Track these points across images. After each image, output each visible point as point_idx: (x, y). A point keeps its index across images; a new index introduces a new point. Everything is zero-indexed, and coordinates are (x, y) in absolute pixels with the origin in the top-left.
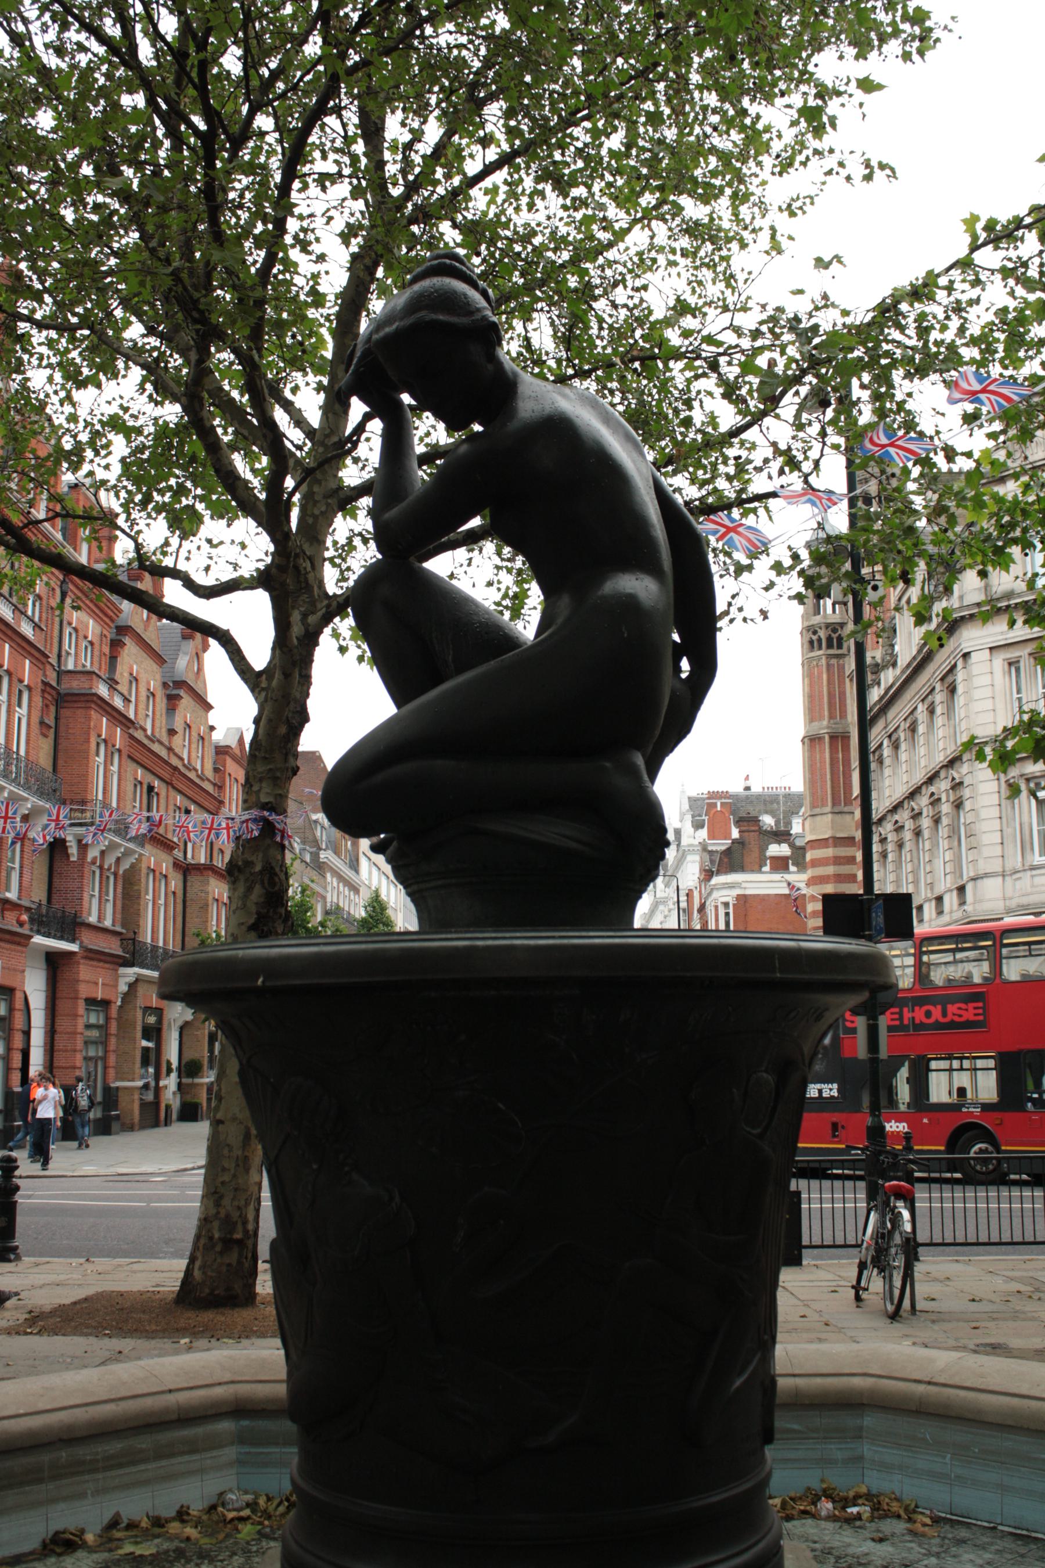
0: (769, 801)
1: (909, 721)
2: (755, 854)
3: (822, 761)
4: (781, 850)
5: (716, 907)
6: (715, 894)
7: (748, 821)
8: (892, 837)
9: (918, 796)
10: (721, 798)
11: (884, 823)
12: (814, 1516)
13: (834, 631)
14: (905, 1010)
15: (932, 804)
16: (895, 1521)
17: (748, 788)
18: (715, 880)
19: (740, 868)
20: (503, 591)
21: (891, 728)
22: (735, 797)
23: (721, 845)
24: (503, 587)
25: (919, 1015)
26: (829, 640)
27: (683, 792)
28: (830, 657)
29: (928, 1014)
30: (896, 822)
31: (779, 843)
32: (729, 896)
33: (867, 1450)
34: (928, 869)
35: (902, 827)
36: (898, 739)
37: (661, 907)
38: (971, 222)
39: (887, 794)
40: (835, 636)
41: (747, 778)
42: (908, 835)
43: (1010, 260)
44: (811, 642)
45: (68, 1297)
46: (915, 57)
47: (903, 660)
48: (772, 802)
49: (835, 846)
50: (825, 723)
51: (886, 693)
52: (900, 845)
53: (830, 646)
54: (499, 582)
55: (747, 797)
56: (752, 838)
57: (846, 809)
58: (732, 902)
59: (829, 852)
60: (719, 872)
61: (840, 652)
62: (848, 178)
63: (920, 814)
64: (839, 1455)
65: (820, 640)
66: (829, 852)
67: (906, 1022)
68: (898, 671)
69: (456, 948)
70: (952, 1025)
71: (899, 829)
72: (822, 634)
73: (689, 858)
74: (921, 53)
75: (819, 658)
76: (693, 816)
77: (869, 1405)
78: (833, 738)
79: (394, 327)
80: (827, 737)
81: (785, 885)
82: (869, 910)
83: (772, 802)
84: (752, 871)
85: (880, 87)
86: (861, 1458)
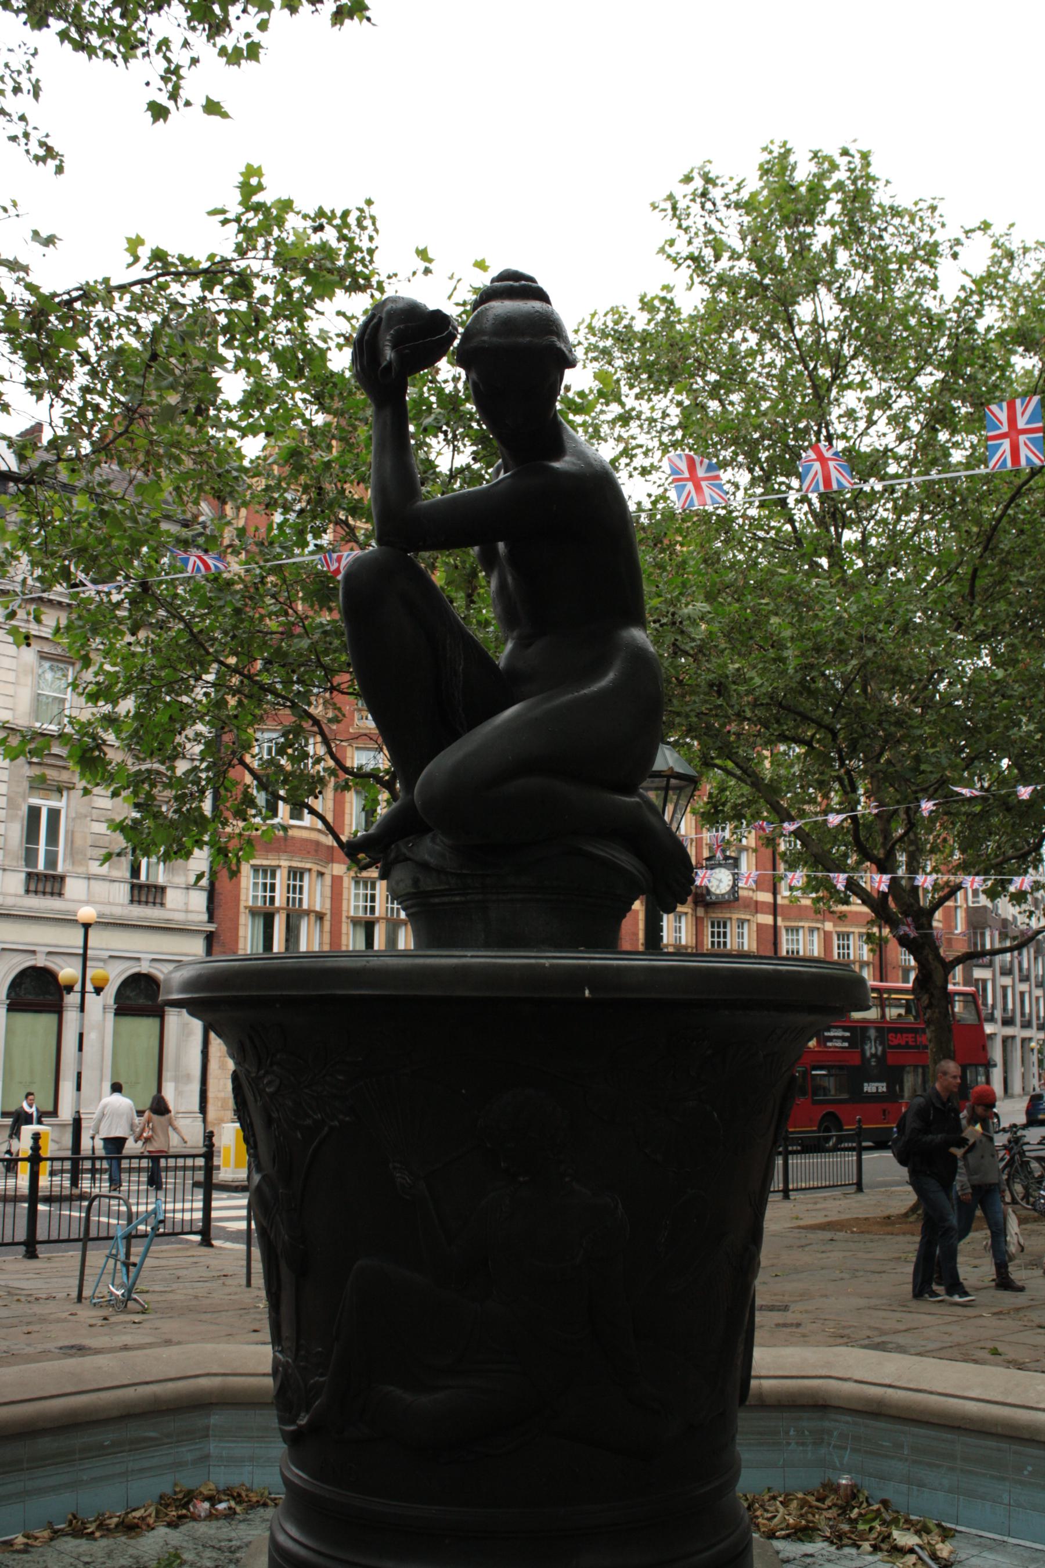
12: (195, 1518)
16: (261, 1510)
33: (213, 1447)
38: (134, 244)
43: (183, 296)
45: (100, 1356)
46: (120, 60)
64: (189, 1457)
69: (514, 965)
77: (217, 1404)
85: (225, 115)
86: (207, 1457)
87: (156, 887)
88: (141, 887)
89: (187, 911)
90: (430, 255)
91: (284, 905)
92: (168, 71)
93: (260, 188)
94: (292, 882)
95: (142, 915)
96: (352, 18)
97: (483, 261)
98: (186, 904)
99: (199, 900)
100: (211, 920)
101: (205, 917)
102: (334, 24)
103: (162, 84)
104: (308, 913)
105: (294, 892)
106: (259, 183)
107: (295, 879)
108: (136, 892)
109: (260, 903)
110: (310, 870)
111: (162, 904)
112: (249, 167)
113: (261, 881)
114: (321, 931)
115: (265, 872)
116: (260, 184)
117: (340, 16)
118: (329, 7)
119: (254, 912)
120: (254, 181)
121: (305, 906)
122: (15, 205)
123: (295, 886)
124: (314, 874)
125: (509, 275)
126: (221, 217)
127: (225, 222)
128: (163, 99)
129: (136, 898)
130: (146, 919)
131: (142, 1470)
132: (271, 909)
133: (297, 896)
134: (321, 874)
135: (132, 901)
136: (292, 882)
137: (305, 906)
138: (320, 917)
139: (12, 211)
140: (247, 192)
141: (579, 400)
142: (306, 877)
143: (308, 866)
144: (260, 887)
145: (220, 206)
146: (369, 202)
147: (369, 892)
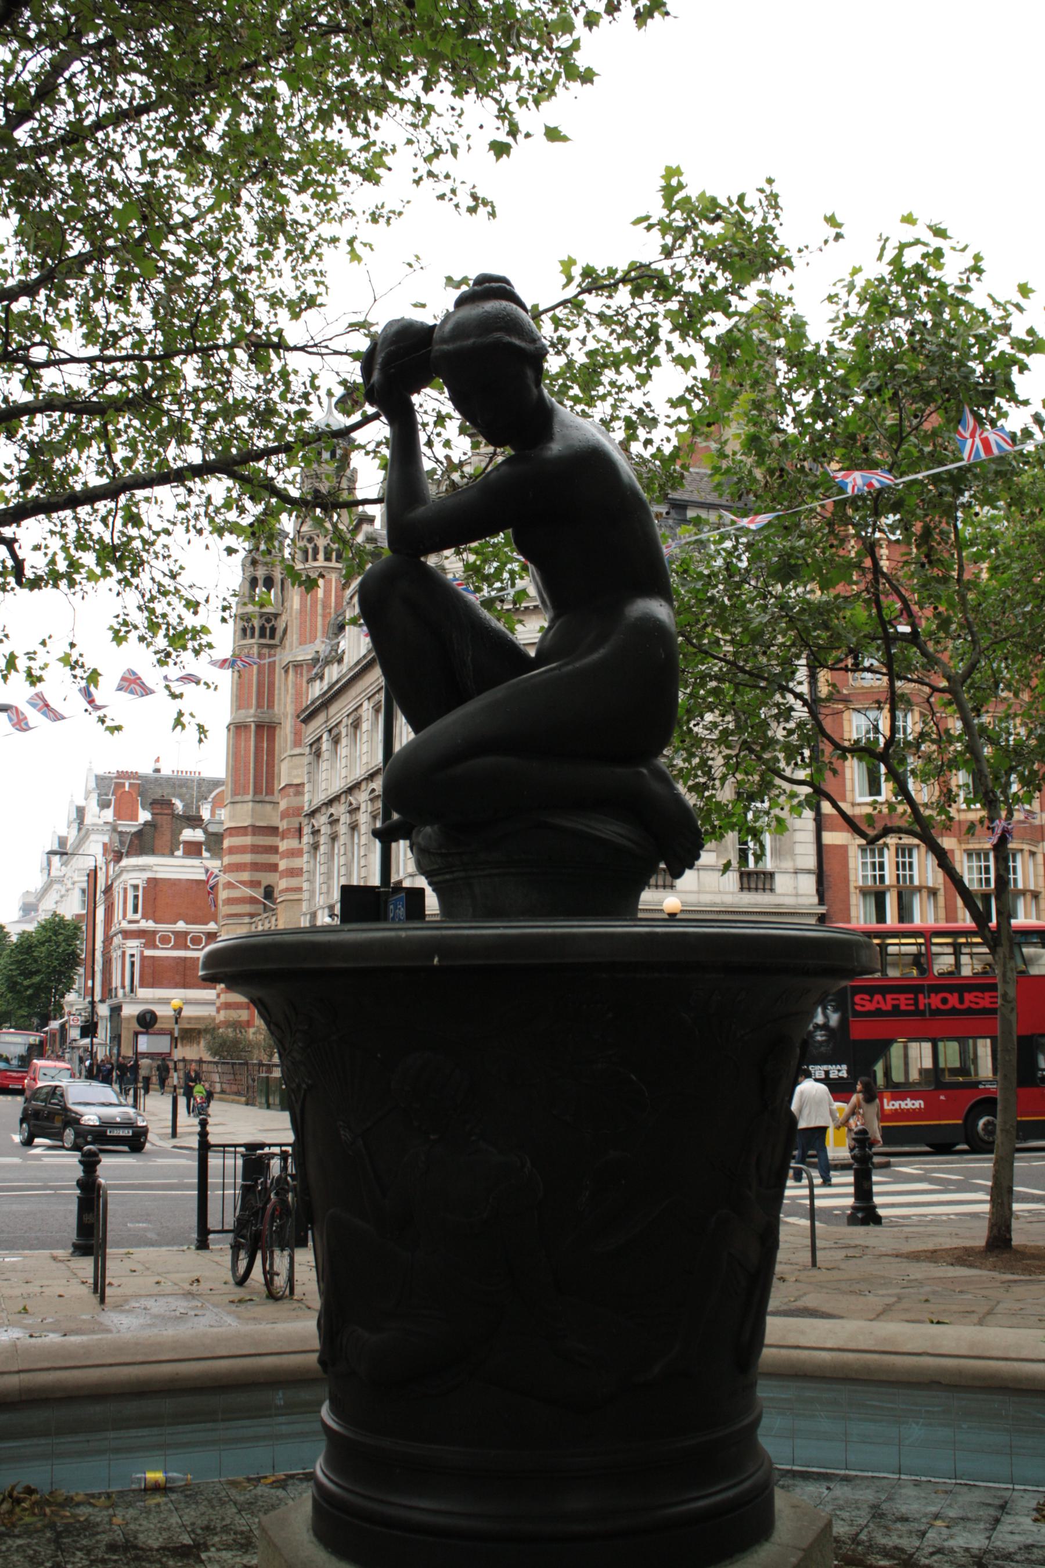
0: (180, 784)
1: (352, 717)
2: (167, 836)
3: (247, 749)
4: (196, 835)
5: (125, 890)
6: (125, 876)
7: (160, 805)
8: (325, 830)
9: (356, 792)
10: (129, 778)
11: (317, 816)
13: (268, 620)
14: (921, 996)
15: (371, 800)
17: (157, 771)
18: (125, 862)
19: (152, 851)
20: (49, 556)
21: (332, 723)
22: (144, 778)
23: (130, 827)
24: (50, 552)
25: (935, 1001)
26: (263, 629)
27: (90, 769)
28: (262, 646)
29: (944, 1001)
30: (332, 815)
31: (194, 827)
32: (139, 879)
34: (363, 863)
35: (338, 820)
36: (339, 734)
37: (56, 886)
38: (567, 265)
39: (323, 786)
40: (268, 626)
41: (158, 760)
42: (342, 829)
43: (609, 307)
44: (244, 630)
46: (531, 104)
47: (350, 659)
48: (181, 786)
49: (254, 834)
50: (252, 711)
51: (330, 688)
52: (334, 838)
53: (262, 635)
54: (46, 547)
55: (156, 779)
56: (165, 821)
57: (267, 799)
58: (141, 884)
59: (248, 840)
60: (129, 854)
61: (272, 642)
62: (457, 206)
63: (358, 809)
65: (253, 628)
66: (248, 840)
67: (921, 1007)
68: (344, 668)
70: (970, 1011)
71: (334, 822)
72: (256, 623)
73: (93, 837)
74: (537, 102)
75: (251, 646)
76: (99, 795)
78: (259, 727)
79: (471, 341)
80: (253, 726)
81: (203, 870)
82: (386, 903)
83: (181, 786)
84: (163, 855)
85: (565, 139)
87: (764, 873)
88: (749, 874)
89: (797, 895)
90: (839, 220)
91: (894, 882)
92: (500, 110)
93: (681, 186)
94: (900, 860)
95: (753, 901)
96: (652, 17)
97: (910, 214)
98: (795, 888)
99: (808, 884)
100: (821, 901)
101: (815, 900)
102: (639, 27)
103: (499, 123)
104: (919, 889)
105: (904, 869)
106: (679, 182)
107: (903, 856)
108: (745, 880)
109: (870, 882)
110: (1022, 850)
111: (772, 890)
112: (668, 169)
113: (869, 860)
114: (936, 907)
115: (978, 855)
116: (680, 183)
117: (642, 17)
118: (627, 11)
119: (864, 892)
120: (674, 182)
121: (1020, 886)
122: (418, 258)
123: (904, 863)
124: (1026, 854)
125: (484, 279)
126: (645, 224)
127: (649, 228)
128: (503, 137)
129: (746, 885)
130: (756, 905)
131: (256, 1438)
132: (881, 888)
133: (908, 873)
134: (1033, 854)
135: (742, 889)
136: (900, 860)
137: (916, 882)
138: (933, 892)
139: (416, 266)
140: (669, 192)
141: (1029, 339)
142: (1019, 858)
143: (1020, 846)
144: (869, 866)
145: (644, 214)
146: (770, 181)
147: (983, 864)
